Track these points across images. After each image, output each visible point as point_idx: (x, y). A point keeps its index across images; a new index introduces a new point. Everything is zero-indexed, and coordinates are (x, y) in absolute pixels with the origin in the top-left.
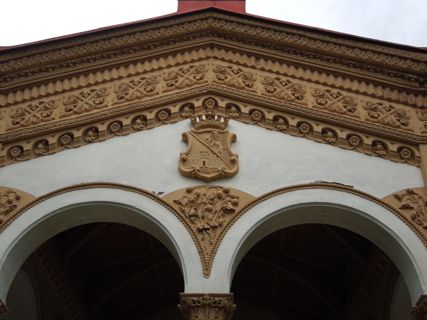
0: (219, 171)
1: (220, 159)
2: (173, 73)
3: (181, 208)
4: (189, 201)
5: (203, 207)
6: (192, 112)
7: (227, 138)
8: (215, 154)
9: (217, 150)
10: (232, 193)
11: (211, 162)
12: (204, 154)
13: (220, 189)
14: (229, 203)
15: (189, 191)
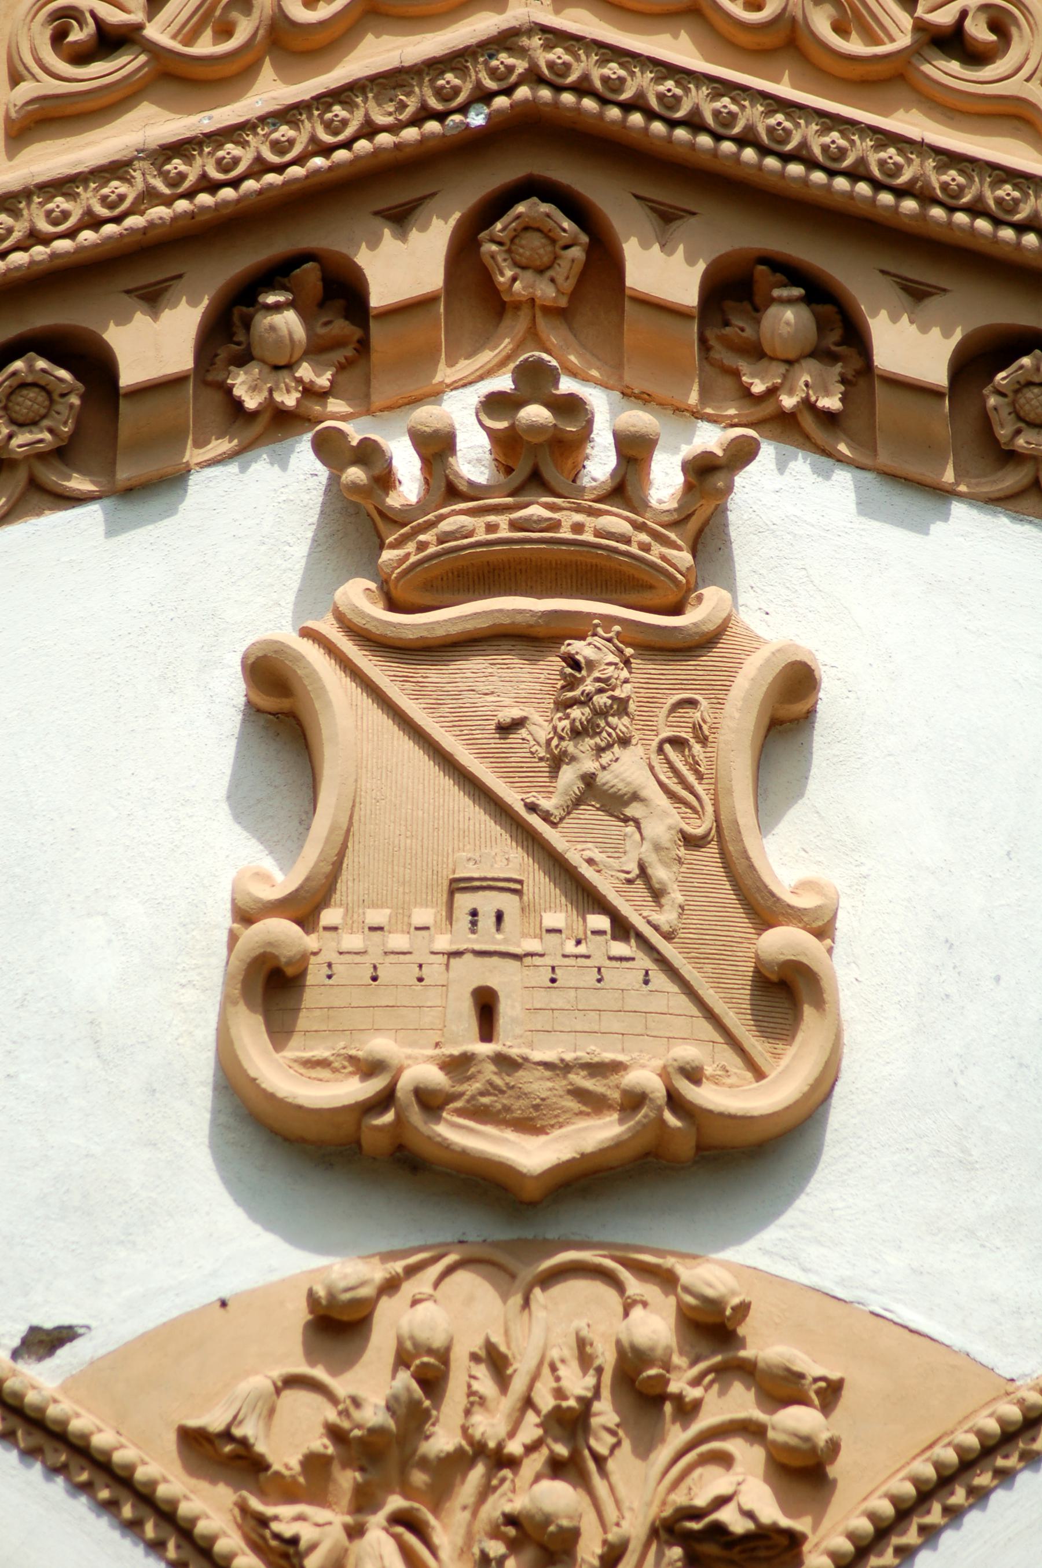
0: (633, 1101)
1: (644, 961)
2: (476, 1386)
3: (263, 1521)
4: (335, 1433)
5: (486, 1491)
6: (336, 344)
7: (718, 703)
8: (586, 897)
9: (617, 850)
10: (765, 1344)
11: (557, 999)
12: (488, 903)
13: (649, 1291)
14: (748, 1456)
15: (337, 1325)
